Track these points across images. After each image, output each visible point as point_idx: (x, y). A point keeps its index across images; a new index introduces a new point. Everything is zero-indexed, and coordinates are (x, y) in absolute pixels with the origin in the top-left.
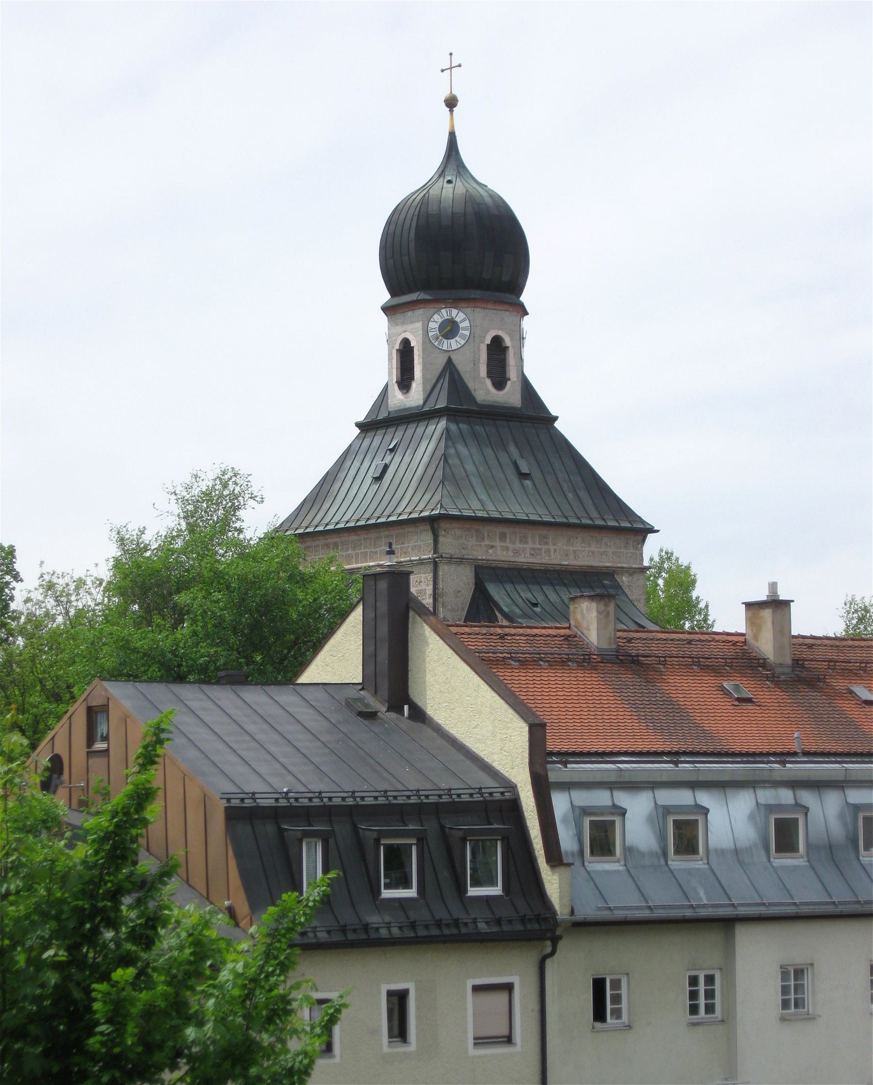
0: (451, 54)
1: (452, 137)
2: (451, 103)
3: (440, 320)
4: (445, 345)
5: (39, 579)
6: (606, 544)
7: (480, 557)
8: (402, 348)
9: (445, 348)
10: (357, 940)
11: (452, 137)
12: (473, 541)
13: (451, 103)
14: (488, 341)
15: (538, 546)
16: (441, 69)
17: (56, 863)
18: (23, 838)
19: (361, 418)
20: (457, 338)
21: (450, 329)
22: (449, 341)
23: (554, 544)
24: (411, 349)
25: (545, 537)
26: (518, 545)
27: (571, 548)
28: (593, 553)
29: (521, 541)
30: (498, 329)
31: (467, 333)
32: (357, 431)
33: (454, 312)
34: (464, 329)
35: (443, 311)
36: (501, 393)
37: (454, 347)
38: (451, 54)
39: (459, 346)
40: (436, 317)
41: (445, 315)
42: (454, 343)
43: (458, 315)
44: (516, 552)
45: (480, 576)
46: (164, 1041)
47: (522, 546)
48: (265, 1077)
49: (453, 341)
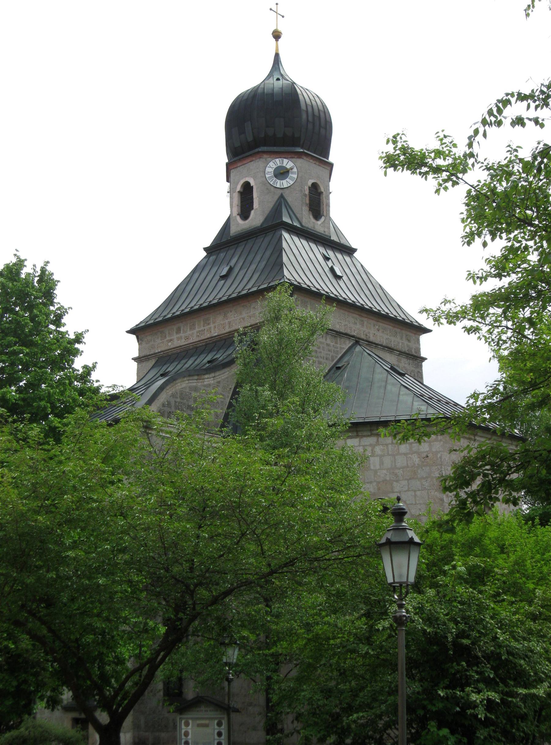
0: (277, 4)
1: (277, 56)
2: (277, 35)
3: (275, 167)
5: (492, 257)
6: (254, 308)
7: (157, 351)
8: (242, 190)
9: (278, 186)
11: (277, 56)
12: (159, 341)
13: (277, 35)
14: (310, 183)
15: (202, 328)
19: (208, 244)
20: (288, 180)
21: (282, 173)
22: (281, 181)
23: (214, 323)
24: (252, 188)
25: (194, 325)
26: (189, 332)
27: (227, 321)
28: (243, 319)
29: (191, 329)
30: (242, 179)
32: (205, 254)
33: (285, 161)
35: (277, 160)
36: (247, 221)
37: (285, 186)
38: (277, 4)
39: (289, 185)
40: (271, 164)
41: (278, 163)
42: (285, 183)
43: (288, 163)
44: (187, 338)
46: (531, 370)
47: (191, 332)
49: (284, 182)
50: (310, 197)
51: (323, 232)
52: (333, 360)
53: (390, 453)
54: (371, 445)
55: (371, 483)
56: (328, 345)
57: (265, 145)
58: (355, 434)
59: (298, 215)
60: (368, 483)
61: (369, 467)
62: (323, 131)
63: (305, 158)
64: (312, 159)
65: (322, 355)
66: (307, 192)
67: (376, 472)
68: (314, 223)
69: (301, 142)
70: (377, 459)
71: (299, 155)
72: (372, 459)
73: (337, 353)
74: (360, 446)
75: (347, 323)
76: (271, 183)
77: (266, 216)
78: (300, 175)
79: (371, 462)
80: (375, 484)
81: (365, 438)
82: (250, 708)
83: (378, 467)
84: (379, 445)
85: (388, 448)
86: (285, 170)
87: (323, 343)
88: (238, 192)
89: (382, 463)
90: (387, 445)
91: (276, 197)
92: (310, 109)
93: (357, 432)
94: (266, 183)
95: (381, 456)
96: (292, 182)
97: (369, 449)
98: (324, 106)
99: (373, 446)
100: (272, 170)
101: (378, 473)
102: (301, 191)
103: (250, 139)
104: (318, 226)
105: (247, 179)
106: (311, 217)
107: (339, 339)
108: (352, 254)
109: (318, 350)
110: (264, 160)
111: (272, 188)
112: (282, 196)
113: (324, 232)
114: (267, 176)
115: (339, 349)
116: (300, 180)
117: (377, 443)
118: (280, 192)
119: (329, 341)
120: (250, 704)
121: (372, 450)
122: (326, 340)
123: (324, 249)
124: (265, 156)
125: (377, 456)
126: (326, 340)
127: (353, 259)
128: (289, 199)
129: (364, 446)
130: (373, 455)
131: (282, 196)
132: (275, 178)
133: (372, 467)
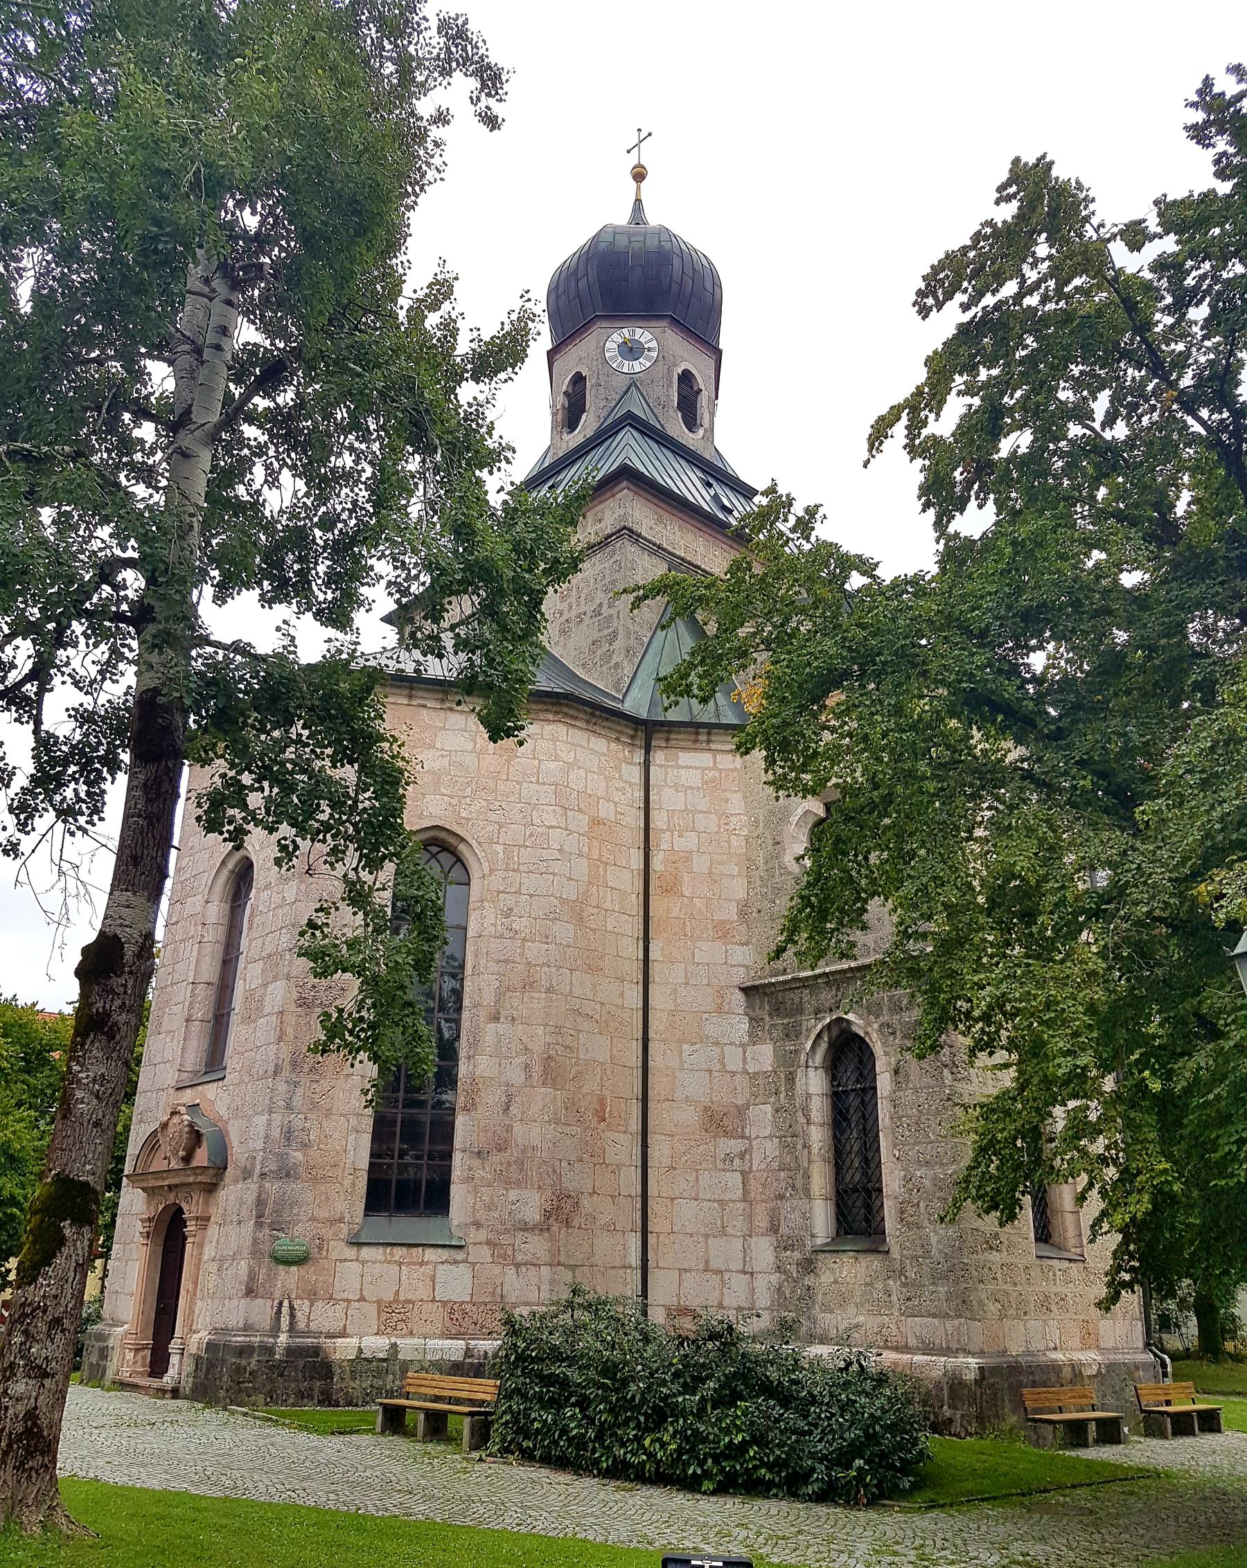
1: (638, 201)
2: (639, 175)
11: (638, 201)
13: (639, 175)
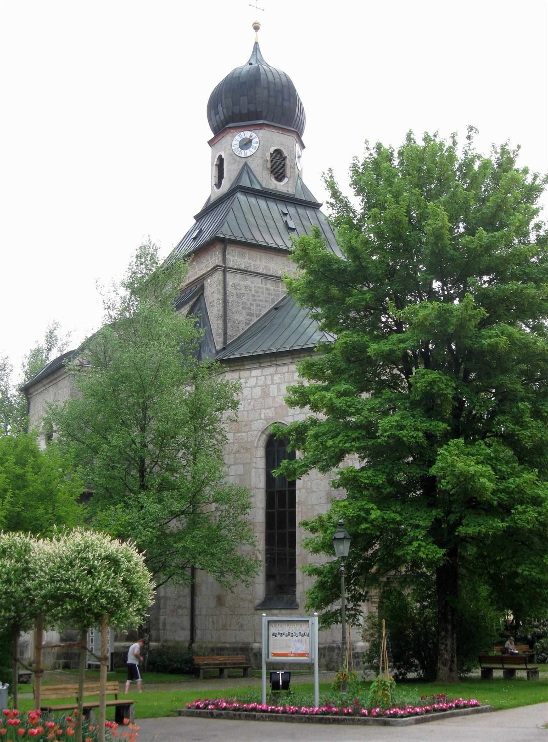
1: (256, 43)
3: (240, 139)
4: (244, 153)
9: (243, 156)
10: (280, 609)
11: (256, 43)
13: (256, 28)
14: (272, 150)
16: (259, 21)
17: (248, 510)
18: (366, 504)
20: (251, 149)
21: (246, 144)
24: (223, 159)
31: (257, 145)
32: (195, 221)
34: (256, 143)
35: (242, 133)
39: (252, 153)
42: (249, 152)
43: (248, 134)
45: (418, 398)
48: (477, 594)
49: (248, 151)
50: (271, 161)
51: (286, 192)
52: (273, 303)
53: (286, 380)
54: (271, 375)
55: (270, 408)
56: (268, 289)
57: (233, 122)
58: (258, 365)
59: (259, 179)
60: (267, 408)
61: (269, 394)
62: (286, 104)
63: (266, 129)
64: (274, 129)
65: (261, 298)
66: (269, 158)
67: (274, 398)
68: (275, 184)
69: (264, 115)
70: (275, 387)
71: (261, 126)
72: (271, 386)
73: (278, 295)
74: (262, 376)
75: (291, 269)
76: (237, 154)
77: (232, 183)
78: (261, 144)
79: (271, 390)
80: (273, 409)
81: (266, 369)
82: (179, 610)
83: (276, 394)
84: (277, 374)
85: (284, 377)
86: (247, 140)
87: (263, 288)
88: (216, 165)
89: (279, 390)
90: (284, 374)
91: (241, 165)
92: (272, 86)
93: (260, 363)
94: (233, 155)
95: (279, 384)
96: (254, 151)
97: (269, 378)
98: (289, 82)
99: (272, 375)
100: (238, 143)
101: (276, 400)
102: (262, 157)
103: (222, 118)
104: (282, 187)
105: (220, 153)
106: (273, 179)
107: (280, 284)
108: (318, 209)
109: (256, 294)
110: (230, 135)
111: (238, 158)
112: (246, 164)
113: (288, 191)
114: (233, 148)
115: (280, 293)
116: (262, 147)
117: (276, 373)
118: (244, 160)
119: (269, 286)
120: (180, 607)
121: (272, 379)
122: (266, 285)
123: (284, 206)
124: (232, 131)
125: (276, 384)
126: (266, 285)
127: (319, 215)
128: (252, 166)
129: (265, 376)
130: (272, 383)
131: (246, 164)
132: (243, 151)
133: (271, 395)
